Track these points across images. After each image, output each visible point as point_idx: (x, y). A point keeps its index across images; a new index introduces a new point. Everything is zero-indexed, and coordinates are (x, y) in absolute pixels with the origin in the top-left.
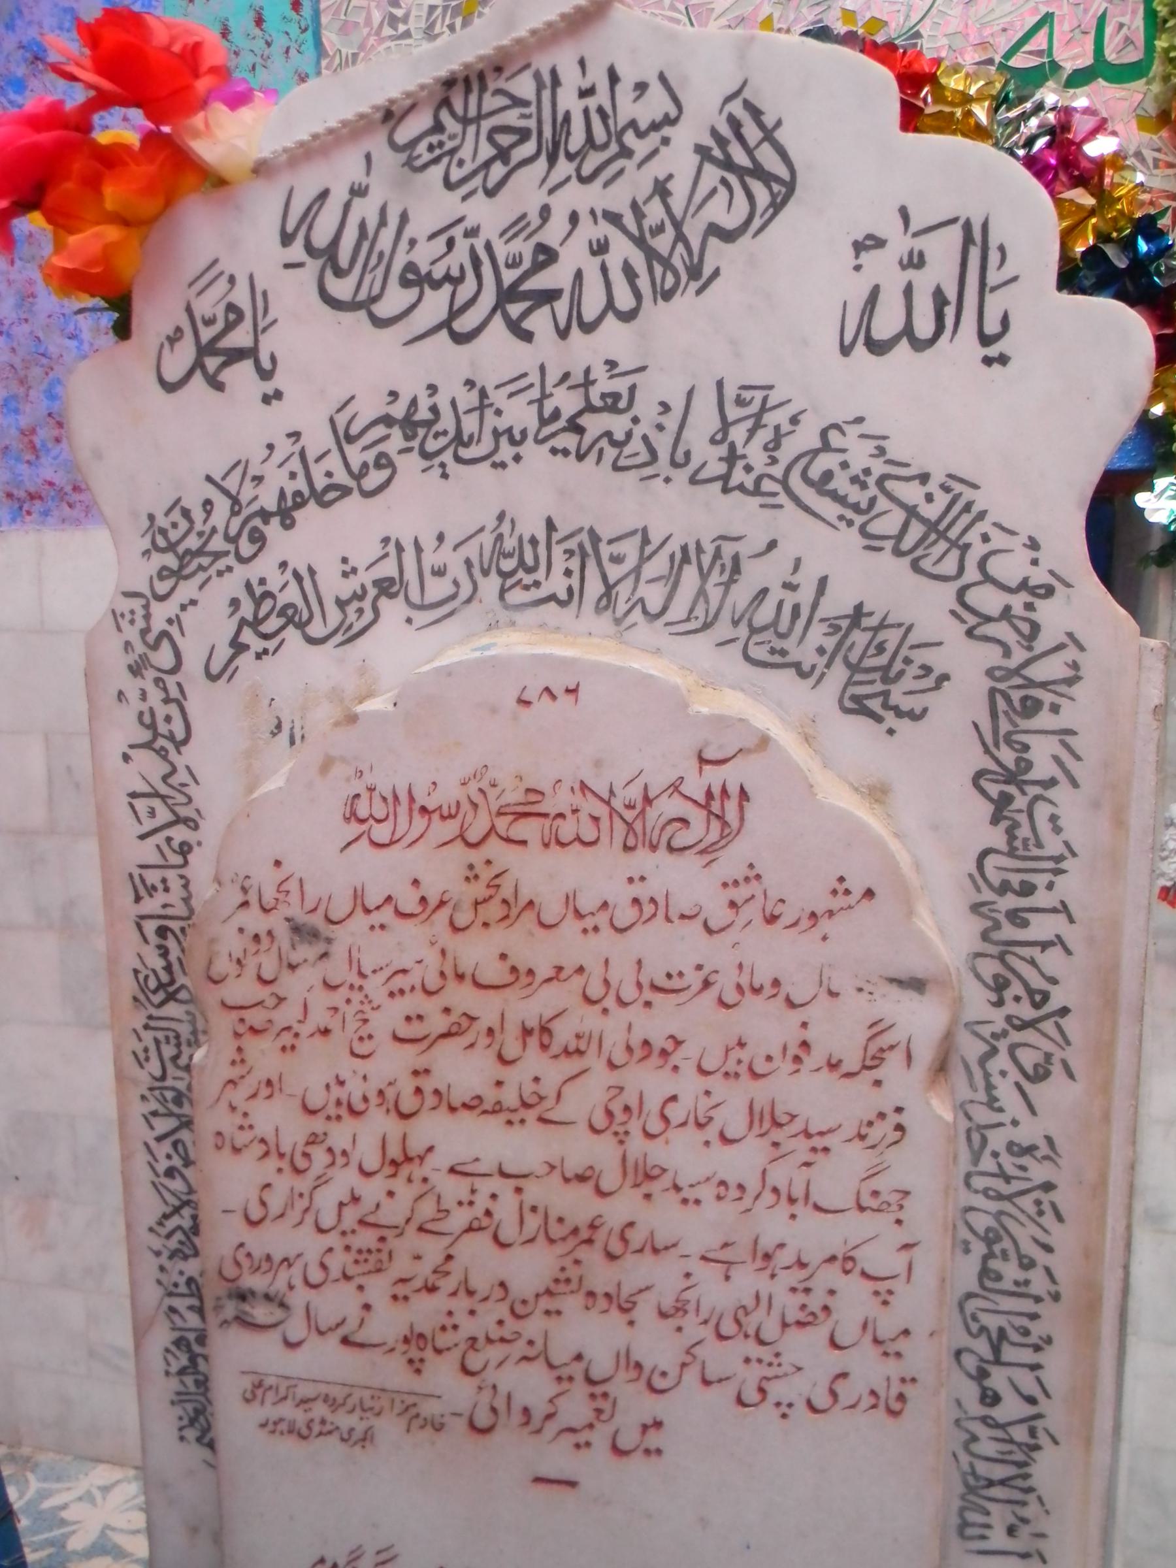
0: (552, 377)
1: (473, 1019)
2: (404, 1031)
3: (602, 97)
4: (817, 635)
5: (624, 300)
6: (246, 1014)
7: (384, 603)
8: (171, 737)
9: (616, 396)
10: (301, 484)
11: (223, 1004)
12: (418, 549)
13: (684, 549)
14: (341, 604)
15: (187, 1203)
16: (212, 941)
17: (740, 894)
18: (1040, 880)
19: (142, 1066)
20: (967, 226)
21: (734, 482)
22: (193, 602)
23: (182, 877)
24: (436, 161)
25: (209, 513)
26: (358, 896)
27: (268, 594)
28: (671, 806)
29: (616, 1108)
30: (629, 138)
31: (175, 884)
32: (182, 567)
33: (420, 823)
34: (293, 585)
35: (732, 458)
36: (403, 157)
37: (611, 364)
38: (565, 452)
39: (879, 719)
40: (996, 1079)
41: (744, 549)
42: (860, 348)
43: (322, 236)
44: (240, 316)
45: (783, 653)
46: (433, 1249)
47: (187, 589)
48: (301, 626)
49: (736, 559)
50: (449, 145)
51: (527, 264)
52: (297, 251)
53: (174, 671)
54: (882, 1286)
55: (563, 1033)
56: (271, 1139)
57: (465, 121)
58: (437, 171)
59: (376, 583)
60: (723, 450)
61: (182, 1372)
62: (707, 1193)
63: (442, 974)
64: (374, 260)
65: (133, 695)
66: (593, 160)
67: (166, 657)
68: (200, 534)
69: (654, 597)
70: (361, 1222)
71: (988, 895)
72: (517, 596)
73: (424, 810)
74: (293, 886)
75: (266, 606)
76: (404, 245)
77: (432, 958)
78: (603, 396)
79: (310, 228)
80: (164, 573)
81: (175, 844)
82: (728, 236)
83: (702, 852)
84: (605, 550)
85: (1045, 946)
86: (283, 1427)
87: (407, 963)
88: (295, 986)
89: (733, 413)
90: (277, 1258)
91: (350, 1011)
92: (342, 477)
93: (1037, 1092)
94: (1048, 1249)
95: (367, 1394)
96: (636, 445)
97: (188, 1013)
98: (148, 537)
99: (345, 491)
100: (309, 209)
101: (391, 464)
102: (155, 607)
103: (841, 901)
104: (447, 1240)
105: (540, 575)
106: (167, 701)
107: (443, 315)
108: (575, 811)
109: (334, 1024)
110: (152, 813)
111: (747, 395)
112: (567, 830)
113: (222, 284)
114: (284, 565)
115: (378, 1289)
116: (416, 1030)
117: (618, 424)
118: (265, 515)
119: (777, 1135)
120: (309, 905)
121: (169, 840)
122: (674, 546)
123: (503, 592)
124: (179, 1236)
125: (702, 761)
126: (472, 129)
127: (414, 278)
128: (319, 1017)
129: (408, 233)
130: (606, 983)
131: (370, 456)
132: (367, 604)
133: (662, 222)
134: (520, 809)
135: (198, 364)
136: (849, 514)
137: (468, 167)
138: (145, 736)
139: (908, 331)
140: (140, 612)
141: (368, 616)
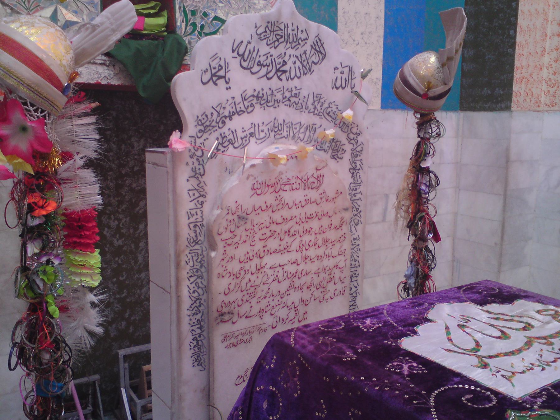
0: (285, 89)
1: (275, 232)
2: (262, 238)
3: (295, 32)
4: (327, 144)
5: (298, 74)
6: (227, 241)
7: (251, 138)
8: (200, 174)
9: (296, 94)
10: (234, 110)
11: (222, 240)
12: (259, 126)
13: (307, 126)
14: (242, 139)
15: (198, 299)
16: (220, 224)
17: (322, 196)
18: (358, 187)
19: (188, 264)
20: (350, 67)
21: (315, 113)
22: (207, 139)
23: (201, 211)
24: (265, 39)
25: (212, 116)
26: (254, 207)
27: (226, 136)
28: (312, 180)
29: (301, 246)
30: (300, 41)
31: (199, 213)
32: (205, 130)
33: (267, 188)
34: (231, 133)
35: (315, 108)
36: (259, 37)
37: (296, 87)
38: (287, 105)
39: (336, 159)
40: (352, 227)
41: (317, 126)
42: (335, 88)
43: (241, 52)
44: (222, 68)
45: (322, 147)
46: (265, 288)
47: (205, 136)
48: (233, 144)
49: (315, 128)
50: (268, 36)
51: (281, 64)
52: (235, 54)
53: (201, 157)
54: (341, 269)
55: (292, 231)
56: (231, 272)
57: (271, 31)
58: (265, 41)
59: (250, 134)
60: (313, 106)
61: (194, 347)
62: (315, 259)
63: (270, 223)
64: (252, 59)
65: (190, 163)
66: (294, 44)
67: (199, 153)
68: (210, 121)
69: (302, 136)
70: (251, 286)
71: (351, 192)
72: (277, 136)
73: (268, 185)
74: (240, 207)
75: (225, 139)
76: (258, 56)
77: (268, 219)
78: (294, 94)
79: (239, 49)
80: (200, 131)
81: (200, 202)
82: (316, 64)
83: (317, 188)
84: (294, 127)
85: (358, 200)
86: (231, 345)
87: (262, 221)
88: (238, 232)
89: (315, 99)
90: (231, 302)
91: (250, 235)
92: (243, 109)
93: (357, 227)
94: (358, 257)
95: (250, 329)
96: (299, 105)
97: (201, 247)
98: (197, 122)
99: (244, 112)
100: (238, 46)
101: (254, 106)
102: (198, 140)
103: (337, 195)
104: (268, 285)
105: (282, 132)
106: (199, 164)
107: (265, 73)
108: (296, 182)
109: (247, 239)
110: (194, 195)
111: (318, 96)
112: (294, 187)
113: (218, 59)
114: (229, 129)
115: (254, 301)
116: (264, 237)
117: (296, 100)
118: (225, 117)
119: (327, 244)
120: (243, 212)
121: (198, 201)
122: (305, 126)
123: (275, 135)
124: (196, 309)
125: (317, 170)
126: (272, 33)
127: (260, 64)
128: (244, 238)
129: (259, 54)
130: (300, 218)
131: (249, 104)
132: (247, 139)
133: (190, 25)
134: (286, 183)
135: (211, 78)
136: (333, 120)
137: (271, 41)
138: (193, 174)
139: (341, 86)
140: (193, 141)
141: (248, 141)
